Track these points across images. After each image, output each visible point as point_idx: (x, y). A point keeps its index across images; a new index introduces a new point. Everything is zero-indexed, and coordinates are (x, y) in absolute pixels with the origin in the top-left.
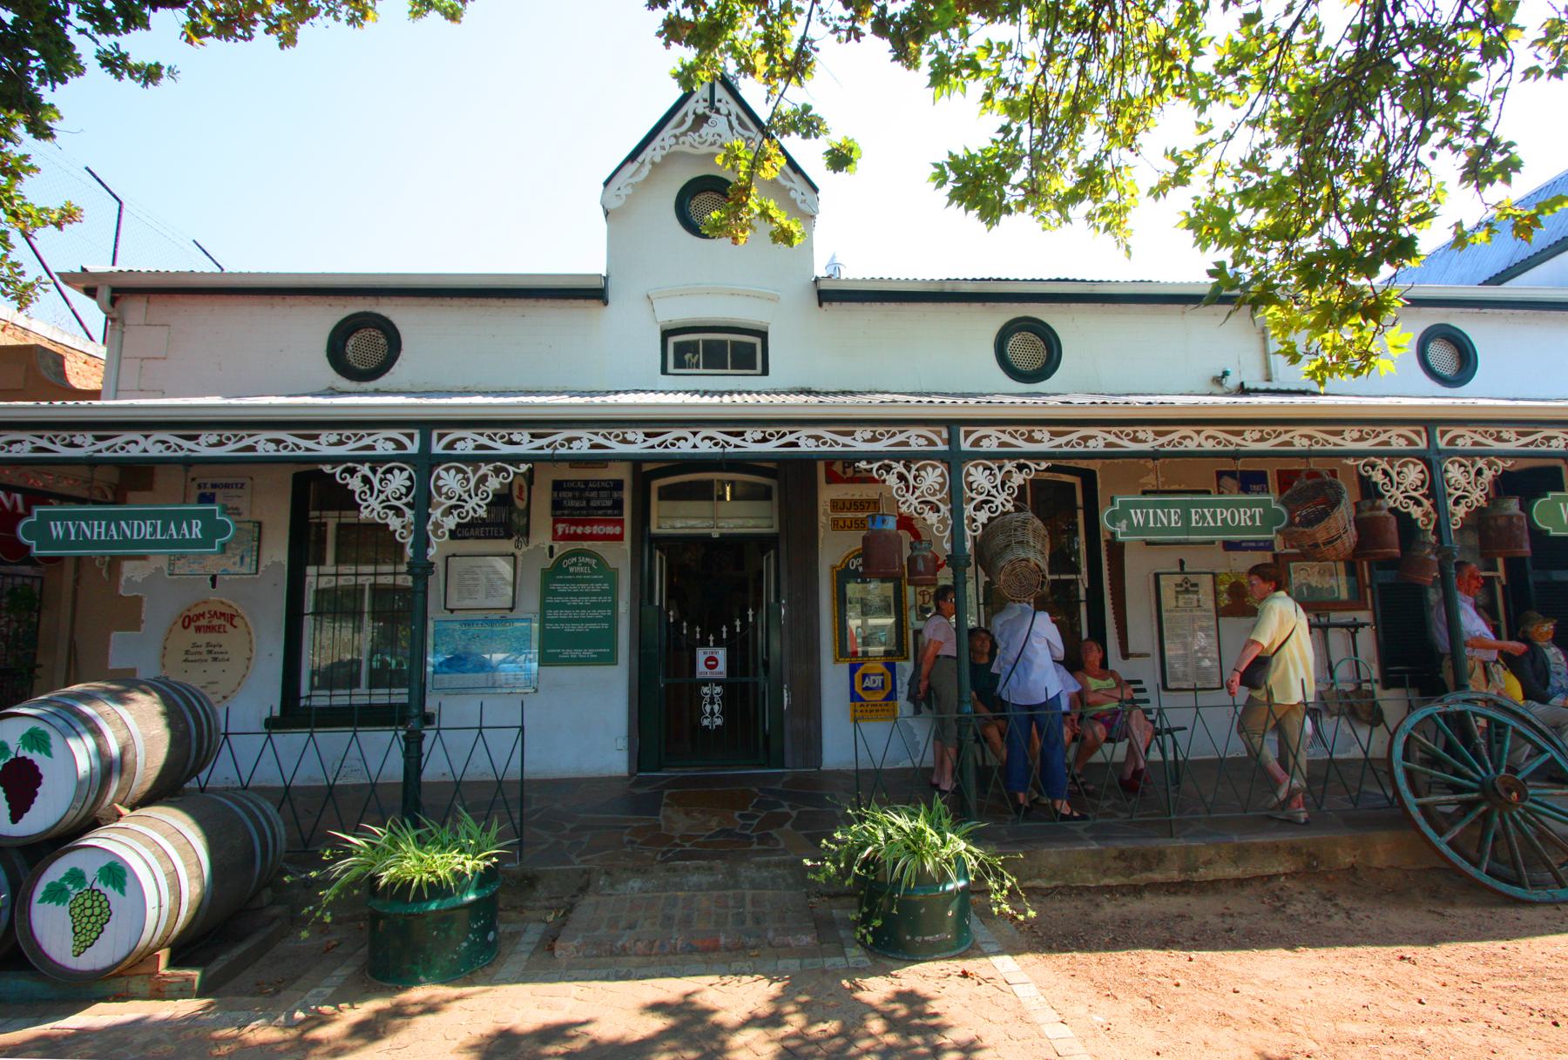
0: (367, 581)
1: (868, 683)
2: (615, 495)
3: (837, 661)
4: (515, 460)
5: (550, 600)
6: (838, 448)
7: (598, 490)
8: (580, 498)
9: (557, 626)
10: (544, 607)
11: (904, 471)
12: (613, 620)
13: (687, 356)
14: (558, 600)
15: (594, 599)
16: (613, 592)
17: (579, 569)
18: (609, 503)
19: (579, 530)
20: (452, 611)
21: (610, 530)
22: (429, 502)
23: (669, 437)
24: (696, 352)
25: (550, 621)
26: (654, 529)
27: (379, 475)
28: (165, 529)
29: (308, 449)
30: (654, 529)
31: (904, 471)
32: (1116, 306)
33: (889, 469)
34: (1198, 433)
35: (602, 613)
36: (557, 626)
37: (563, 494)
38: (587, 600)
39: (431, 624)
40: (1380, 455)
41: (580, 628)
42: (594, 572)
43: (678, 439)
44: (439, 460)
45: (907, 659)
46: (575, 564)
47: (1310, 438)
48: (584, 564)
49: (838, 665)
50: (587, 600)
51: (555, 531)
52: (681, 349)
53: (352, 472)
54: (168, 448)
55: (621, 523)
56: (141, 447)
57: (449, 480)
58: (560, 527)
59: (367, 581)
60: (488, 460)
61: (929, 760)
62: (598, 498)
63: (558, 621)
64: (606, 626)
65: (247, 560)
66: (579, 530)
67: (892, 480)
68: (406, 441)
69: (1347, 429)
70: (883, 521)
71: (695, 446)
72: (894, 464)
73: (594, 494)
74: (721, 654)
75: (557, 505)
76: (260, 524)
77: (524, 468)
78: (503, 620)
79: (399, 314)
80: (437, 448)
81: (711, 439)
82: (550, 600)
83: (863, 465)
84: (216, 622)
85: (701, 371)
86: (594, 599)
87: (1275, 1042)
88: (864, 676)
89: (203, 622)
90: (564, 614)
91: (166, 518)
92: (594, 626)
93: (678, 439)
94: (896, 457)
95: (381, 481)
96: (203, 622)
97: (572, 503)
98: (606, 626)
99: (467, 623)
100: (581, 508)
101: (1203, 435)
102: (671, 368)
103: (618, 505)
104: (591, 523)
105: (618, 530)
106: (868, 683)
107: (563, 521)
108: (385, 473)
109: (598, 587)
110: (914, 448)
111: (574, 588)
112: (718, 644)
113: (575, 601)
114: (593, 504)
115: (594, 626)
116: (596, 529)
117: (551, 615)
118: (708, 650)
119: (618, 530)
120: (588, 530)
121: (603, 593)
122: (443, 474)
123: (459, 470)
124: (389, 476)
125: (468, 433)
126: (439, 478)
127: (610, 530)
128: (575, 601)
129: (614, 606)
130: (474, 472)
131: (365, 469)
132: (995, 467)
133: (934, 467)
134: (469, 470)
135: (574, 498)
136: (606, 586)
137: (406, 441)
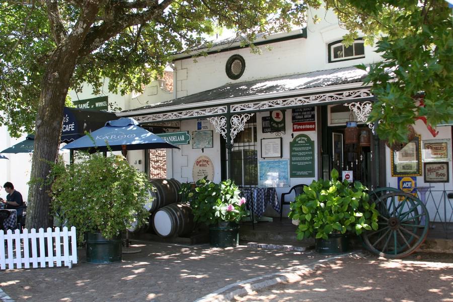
0: (242, 148)
1: (405, 185)
2: (312, 113)
3: (392, 176)
4: (250, 112)
5: (293, 153)
6: (306, 104)
7: (306, 111)
8: (301, 115)
9: (295, 163)
10: (291, 156)
11: (359, 106)
12: (313, 160)
13: (339, 53)
14: (295, 153)
15: (307, 153)
16: (313, 150)
17: (301, 142)
18: (310, 116)
19: (301, 127)
20: (264, 158)
21: (311, 126)
22: (231, 127)
23: (289, 101)
24: (342, 50)
25: (294, 161)
26: (329, 125)
27: (362, 106)
28: (177, 138)
29: (340, 99)
30: (329, 125)
31: (359, 106)
32: (302, 77)
33: (354, 105)
34: (296, 99)
35: (308, 158)
36: (295, 163)
37: (296, 114)
38: (304, 153)
39: (258, 165)
40: (356, 101)
41: (302, 164)
42: (306, 143)
43: (291, 102)
44: (233, 114)
45: (421, 175)
46: (300, 140)
47: (197, 112)
48: (303, 140)
49: (394, 178)
50: (304, 153)
51: (293, 128)
52: (336, 50)
53: (354, 105)
54: (334, 99)
55: (314, 124)
56: (294, 103)
57: (235, 120)
58: (295, 126)
59: (242, 148)
60: (244, 113)
61: (424, 224)
62: (307, 114)
63: (296, 161)
64: (310, 163)
65: (210, 143)
66: (301, 127)
67: (355, 109)
68: (224, 109)
69: (344, 92)
70: (350, 124)
71: (296, 104)
72: (356, 104)
73: (305, 113)
74: (351, 173)
75: (294, 118)
76: (213, 131)
77: (252, 115)
78: (279, 162)
79: (244, 53)
80: (232, 111)
81: (300, 100)
82: (293, 153)
83: (346, 105)
84: (204, 163)
85: (344, 58)
86: (307, 153)
87: (427, 301)
88: (404, 182)
89: (201, 163)
90: (298, 159)
91: (177, 135)
92: (307, 163)
93: (291, 102)
94: (356, 101)
95: (363, 108)
96: (201, 163)
97: (298, 117)
98: (310, 163)
99: (268, 162)
100: (302, 119)
101: (297, 100)
102: (333, 59)
103: (313, 116)
104: (305, 124)
105: (313, 126)
106: (405, 185)
107: (296, 124)
108: (364, 105)
109: (307, 148)
110: (362, 97)
111: (300, 149)
112: (350, 169)
113: (301, 154)
114: (305, 117)
115: (307, 163)
116: (308, 127)
117: (294, 159)
118: (346, 172)
119: (313, 126)
120: (304, 127)
121: (309, 150)
122: (233, 118)
123: (237, 117)
124: (365, 106)
125: (238, 105)
126: (224, 118)
127: (311, 126)
128: (301, 154)
129: (313, 155)
130: (240, 117)
131: (358, 104)
132: (239, 116)
133: (232, 120)
134: (239, 116)
135: (299, 115)
136: (310, 148)
137: (224, 109)
